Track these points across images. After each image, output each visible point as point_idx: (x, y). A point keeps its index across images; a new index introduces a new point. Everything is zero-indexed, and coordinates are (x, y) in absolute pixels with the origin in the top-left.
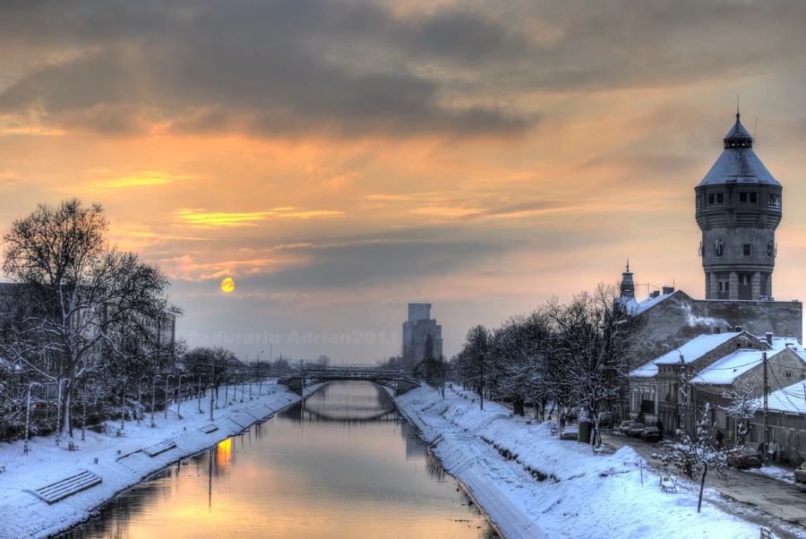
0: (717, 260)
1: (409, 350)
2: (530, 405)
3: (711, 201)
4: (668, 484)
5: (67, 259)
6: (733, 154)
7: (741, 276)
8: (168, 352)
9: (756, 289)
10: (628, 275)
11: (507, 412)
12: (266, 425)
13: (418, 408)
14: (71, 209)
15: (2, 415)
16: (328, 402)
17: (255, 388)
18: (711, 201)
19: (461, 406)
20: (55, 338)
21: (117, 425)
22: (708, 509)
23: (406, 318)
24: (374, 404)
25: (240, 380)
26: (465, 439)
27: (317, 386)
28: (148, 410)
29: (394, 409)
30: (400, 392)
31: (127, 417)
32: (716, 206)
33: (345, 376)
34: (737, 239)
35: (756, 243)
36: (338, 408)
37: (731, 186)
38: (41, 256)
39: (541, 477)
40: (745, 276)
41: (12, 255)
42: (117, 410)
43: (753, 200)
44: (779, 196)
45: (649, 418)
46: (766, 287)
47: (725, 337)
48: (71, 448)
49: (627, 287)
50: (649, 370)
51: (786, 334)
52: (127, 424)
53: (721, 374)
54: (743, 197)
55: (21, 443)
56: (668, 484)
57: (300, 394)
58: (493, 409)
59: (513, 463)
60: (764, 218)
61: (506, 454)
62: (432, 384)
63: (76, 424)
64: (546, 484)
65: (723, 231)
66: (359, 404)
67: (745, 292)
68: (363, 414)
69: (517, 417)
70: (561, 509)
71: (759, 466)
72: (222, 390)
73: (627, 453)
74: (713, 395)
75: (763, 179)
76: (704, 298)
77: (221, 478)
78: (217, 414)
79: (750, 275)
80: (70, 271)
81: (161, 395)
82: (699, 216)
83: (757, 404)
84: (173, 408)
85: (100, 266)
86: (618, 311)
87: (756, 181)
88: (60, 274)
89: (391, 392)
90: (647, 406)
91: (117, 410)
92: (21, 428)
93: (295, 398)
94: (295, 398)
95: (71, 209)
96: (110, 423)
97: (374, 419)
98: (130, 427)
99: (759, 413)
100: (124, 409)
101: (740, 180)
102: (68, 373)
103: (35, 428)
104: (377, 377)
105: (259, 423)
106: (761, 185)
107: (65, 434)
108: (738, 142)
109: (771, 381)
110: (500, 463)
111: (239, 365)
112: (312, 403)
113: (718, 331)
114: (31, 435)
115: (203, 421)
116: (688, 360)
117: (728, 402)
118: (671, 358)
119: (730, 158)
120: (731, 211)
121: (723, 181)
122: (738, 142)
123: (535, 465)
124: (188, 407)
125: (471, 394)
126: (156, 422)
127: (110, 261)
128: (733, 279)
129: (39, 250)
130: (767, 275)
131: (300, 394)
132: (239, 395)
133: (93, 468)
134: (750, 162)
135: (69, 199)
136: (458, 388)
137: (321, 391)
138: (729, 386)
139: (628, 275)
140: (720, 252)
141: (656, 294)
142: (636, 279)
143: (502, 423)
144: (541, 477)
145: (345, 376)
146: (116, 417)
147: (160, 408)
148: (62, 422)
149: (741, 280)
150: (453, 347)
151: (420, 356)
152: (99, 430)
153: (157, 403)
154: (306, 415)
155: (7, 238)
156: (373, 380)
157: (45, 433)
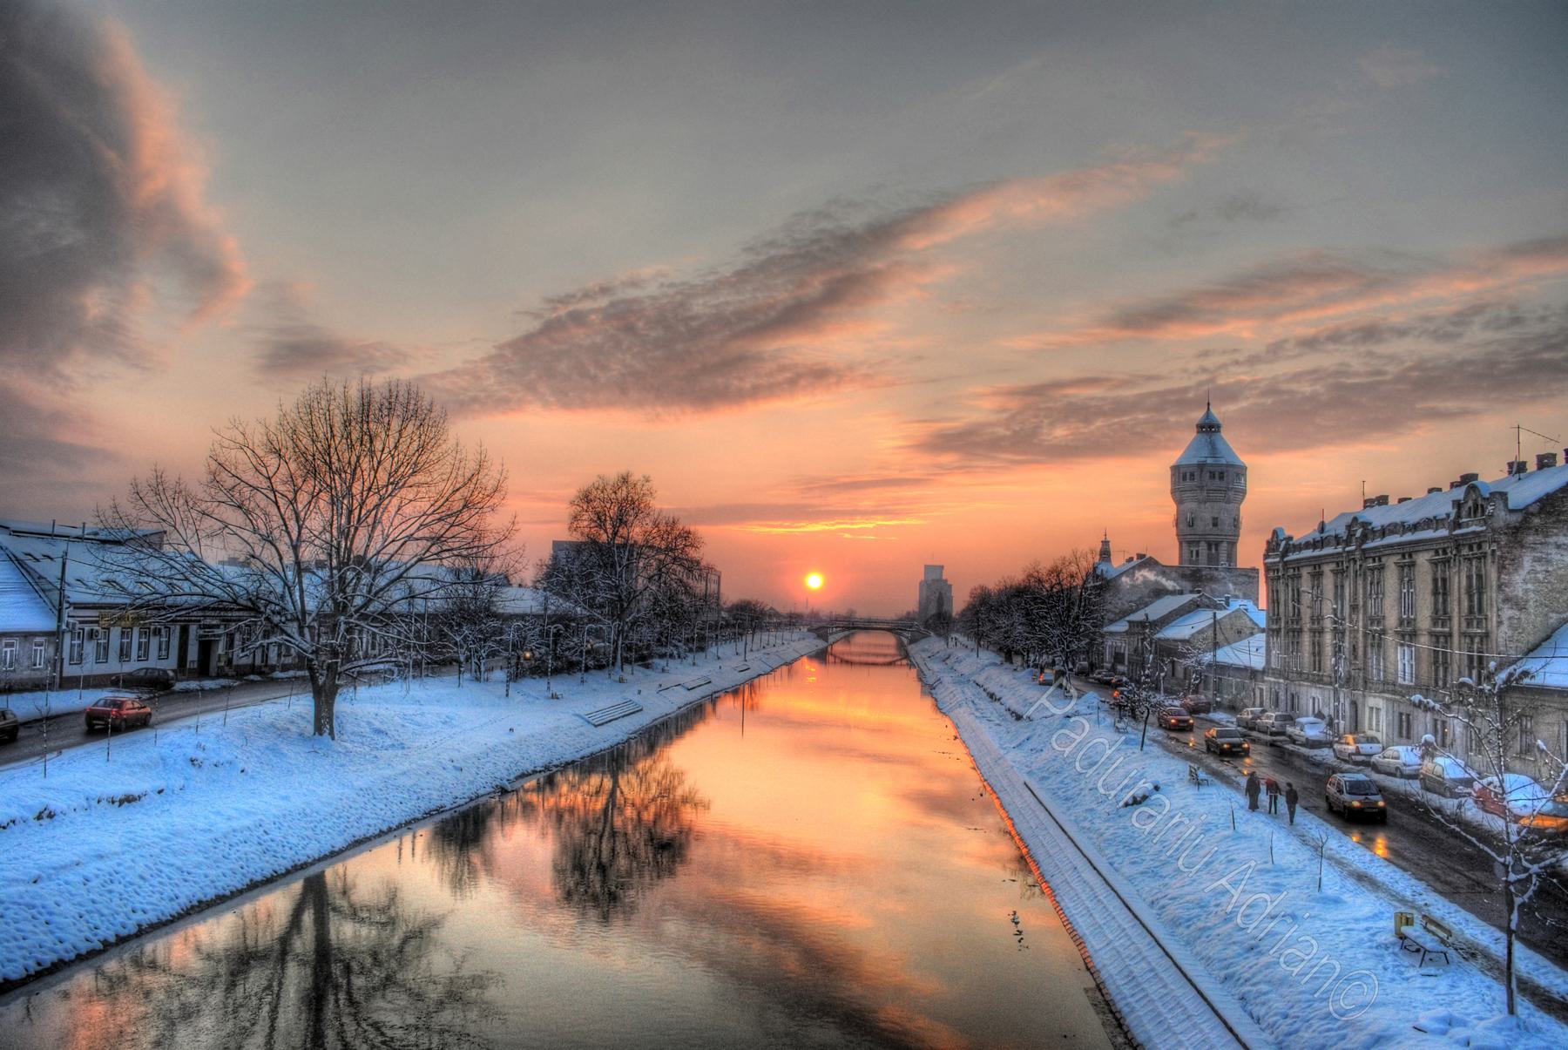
0: (1188, 530)
1: (923, 606)
2: (1017, 653)
3: (1184, 478)
4: (1120, 725)
5: (621, 521)
6: (1205, 437)
7: (1209, 545)
8: (709, 600)
9: (1223, 556)
10: (1105, 543)
11: (998, 659)
12: (796, 665)
13: (925, 655)
14: (625, 480)
15: (373, 1046)
16: (854, 649)
17: (787, 635)
18: (1184, 478)
19: (960, 654)
20: (610, 588)
21: (662, 662)
22: (465, 684)
23: (922, 577)
24: (893, 651)
25: (778, 626)
26: (959, 682)
27: (842, 634)
28: (691, 650)
29: (907, 656)
30: (912, 641)
31: (671, 656)
32: (1188, 483)
33: (868, 626)
34: (1207, 513)
35: (1223, 516)
36: (860, 654)
37: (1201, 466)
38: (600, 520)
39: (1019, 718)
40: (1213, 545)
41: (576, 518)
42: (663, 650)
43: (1221, 478)
44: (1245, 475)
45: (1120, 668)
46: (1231, 557)
47: (1188, 598)
48: (621, 681)
49: (1105, 554)
50: (1121, 627)
51: (1246, 596)
52: (671, 663)
53: (1179, 631)
54: (1212, 476)
55: (579, 675)
56: (1120, 725)
57: (826, 640)
58: (987, 656)
59: (997, 704)
60: (1231, 494)
61: (992, 696)
62: (939, 635)
63: (626, 661)
64: (1021, 723)
65: (1194, 505)
66: (879, 651)
67: (1213, 559)
68: (881, 660)
69: (1007, 665)
70: (1029, 746)
71: (1208, 711)
72: (757, 637)
73: (1093, 697)
74: (1168, 651)
75: (1231, 460)
76: (1176, 563)
77: (475, 686)
78: (749, 656)
79: (1217, 545)
80: (623, 531)
81: (702, 638)
82: (1173, 492)
83: (1208, 658)
84: (713, 650)
85: (649, 528)
86: (1094, 573)
87: (1223, 461)
88: (615, 534)
89: (905, 641)
90: (1118, 658)
91: (663, 650)
92: (579, 663)
93: (821, 644)
94: (821, 644)
95: (625, 480)
96: (656, 661)
97: (890, 664)
98: (673, 664)
99: (1209, 665)
100: (670, 649)
101: (1209, 461)
102: (620, 618)
103: (591, 663)
104: (896, 628)
105: (789, 664)
106: (1229, 465)
107: (617, 668)
108: (1209, 428)
109: (1220, 638)
110: (985, 704)
111: (777, 615)
112: (839, 648)
113: (1181, 593)
114: (587, 669)
115: (738, 662)
116: (1151, 618)
117: (1183, 656)
118: (1138, 616)
119: (1516, 320)
120: (1201, 488)
121: (1195, 461)
122: (1209, 428)
123: (1015, 707)
124: (726, 649)
125: (972, 644)
126: (625, 677)
127: (656, 524)
128: (1203, 547)
129: (597, 514)
130: (1233, 545)
131: (826, 640)
132: (772, 641)
133: (636, 698)
134: (1220, 446)
135: (623, 471)
136: (962, 639)
137: (847, 639)
138: (1184, 641)
139: (1105, 543)
140: (1191, 524)
141: (1131, 559)
142: (1112, 547)
143: (993, 671)
144: (1019, 718)
145: (868, 626)
146: (662, 656)
147: (701, 649)
148: (615, 658)
149: (1210, 548)
150: (959, 602)
151: (933, 610)
152: (647, 666)
153: (699, 644)
154: (831, 659)
155: (572, 503)
156: (889, 630)
157: (600, 667)
